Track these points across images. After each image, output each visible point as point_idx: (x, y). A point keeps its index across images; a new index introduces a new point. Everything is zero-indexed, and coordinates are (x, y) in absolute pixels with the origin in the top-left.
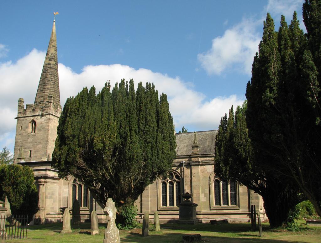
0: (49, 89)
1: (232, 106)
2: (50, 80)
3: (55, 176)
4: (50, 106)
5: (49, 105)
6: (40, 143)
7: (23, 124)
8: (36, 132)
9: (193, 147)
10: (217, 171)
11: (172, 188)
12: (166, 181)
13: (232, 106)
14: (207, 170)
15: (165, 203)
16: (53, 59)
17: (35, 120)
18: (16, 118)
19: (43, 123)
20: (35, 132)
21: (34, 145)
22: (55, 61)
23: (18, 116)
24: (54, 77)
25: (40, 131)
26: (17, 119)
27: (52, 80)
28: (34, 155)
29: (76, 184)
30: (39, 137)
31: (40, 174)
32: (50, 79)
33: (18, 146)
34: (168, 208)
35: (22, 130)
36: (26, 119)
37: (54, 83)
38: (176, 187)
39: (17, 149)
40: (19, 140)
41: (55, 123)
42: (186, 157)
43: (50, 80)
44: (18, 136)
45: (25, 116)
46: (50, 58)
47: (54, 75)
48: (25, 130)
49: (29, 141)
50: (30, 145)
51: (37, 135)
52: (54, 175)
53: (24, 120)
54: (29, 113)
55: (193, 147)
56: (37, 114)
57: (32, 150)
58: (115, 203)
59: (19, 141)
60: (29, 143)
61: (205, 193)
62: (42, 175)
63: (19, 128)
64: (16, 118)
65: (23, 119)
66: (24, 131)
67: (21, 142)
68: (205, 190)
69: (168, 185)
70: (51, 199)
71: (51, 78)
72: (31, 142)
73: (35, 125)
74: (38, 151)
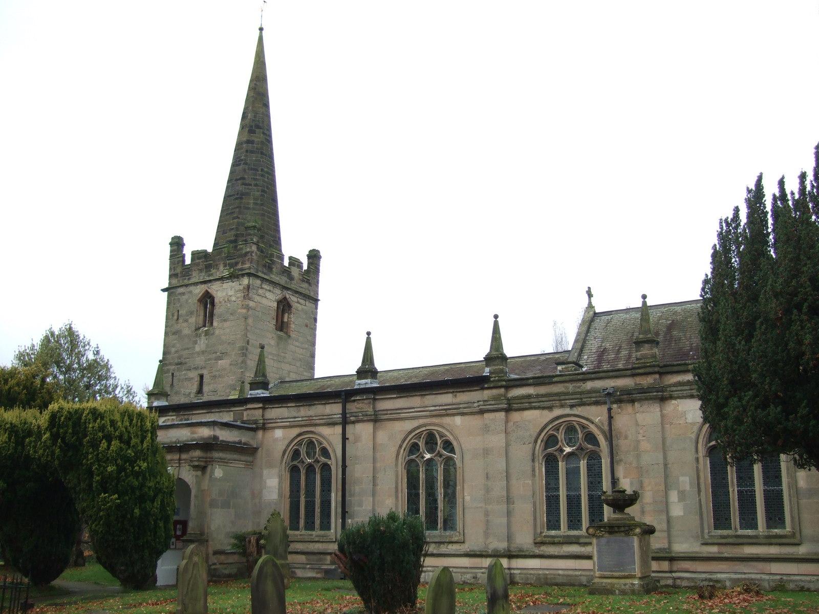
0: (248, 208)
1: (760, 179)
2: (251, 185)
3: (240, 442)
4: (248, 252)
5: (248, 250)
6: (224, 355)
7: (181, 306)
8: (215, 324)
9: (639, 343)
10: (714, 413)
11: (572, 474)
12: (556, 453)
13: (760, 179)
14: (684, 414)
15: (553, 523)
16: (258, 127)
17: (214, 293)
18: (164, 290)
19: (234, 299)
20: (212, 324)
21: (209, 360)
22: (264, 133)
23: (170, 283)
24: (262, 176)
25: (225, 321)
26: (166, 293)
27: (256, 185)
28: (211, 387)
29: (300, 466)
30: (223, 338)
31: (196, 436)
32: (253, 182)
33: (171, 364)
34: (564, 537)
35: (181, 320)
36: (190, 292)
37: (263, 191)
38: (382, 395)
39: (168, 371)
40: (173, 346)
41: (266, 297)
42: (745, 540)
43: (251, 185)
44: (172, 337)
45: (186, 282)
46: (252, 126)
47: (262, 170)
48: (186, 321)
49: (197, 349)
50: (199, 361)
51: (217, 332)
52: (237, 439)
53: (183, 294)
54: (196, 277)
55: (639, 343)
56: (218, 275)
57: (205, 372)
58: (385, 517)
59: (173, 350)
60: (198, 353)
61: (681, 489)
62: (202, 439)
63: (173, 315)
64: (164, 290)
65: (181, 290)
66: (185, 324)
67: (176, 352)
68: (681, 479)
69: (562, 465)
70: (230, 508)
71: (255, 179)
72: (203, 352)
73: (213, 304)
74: (220, 376)
